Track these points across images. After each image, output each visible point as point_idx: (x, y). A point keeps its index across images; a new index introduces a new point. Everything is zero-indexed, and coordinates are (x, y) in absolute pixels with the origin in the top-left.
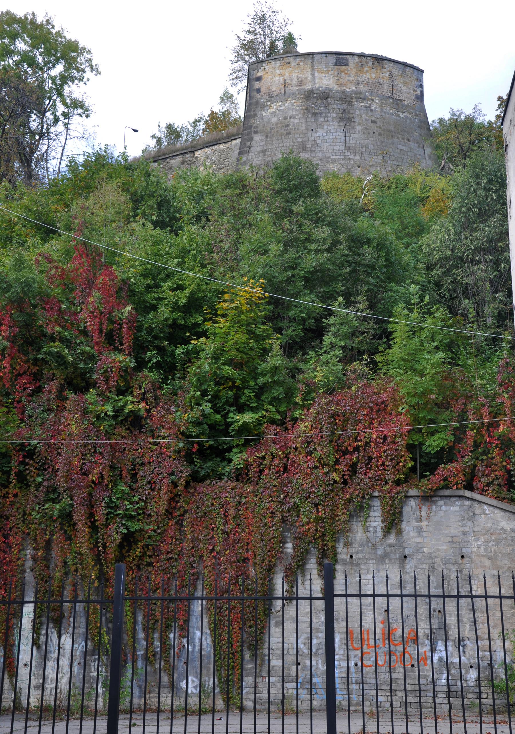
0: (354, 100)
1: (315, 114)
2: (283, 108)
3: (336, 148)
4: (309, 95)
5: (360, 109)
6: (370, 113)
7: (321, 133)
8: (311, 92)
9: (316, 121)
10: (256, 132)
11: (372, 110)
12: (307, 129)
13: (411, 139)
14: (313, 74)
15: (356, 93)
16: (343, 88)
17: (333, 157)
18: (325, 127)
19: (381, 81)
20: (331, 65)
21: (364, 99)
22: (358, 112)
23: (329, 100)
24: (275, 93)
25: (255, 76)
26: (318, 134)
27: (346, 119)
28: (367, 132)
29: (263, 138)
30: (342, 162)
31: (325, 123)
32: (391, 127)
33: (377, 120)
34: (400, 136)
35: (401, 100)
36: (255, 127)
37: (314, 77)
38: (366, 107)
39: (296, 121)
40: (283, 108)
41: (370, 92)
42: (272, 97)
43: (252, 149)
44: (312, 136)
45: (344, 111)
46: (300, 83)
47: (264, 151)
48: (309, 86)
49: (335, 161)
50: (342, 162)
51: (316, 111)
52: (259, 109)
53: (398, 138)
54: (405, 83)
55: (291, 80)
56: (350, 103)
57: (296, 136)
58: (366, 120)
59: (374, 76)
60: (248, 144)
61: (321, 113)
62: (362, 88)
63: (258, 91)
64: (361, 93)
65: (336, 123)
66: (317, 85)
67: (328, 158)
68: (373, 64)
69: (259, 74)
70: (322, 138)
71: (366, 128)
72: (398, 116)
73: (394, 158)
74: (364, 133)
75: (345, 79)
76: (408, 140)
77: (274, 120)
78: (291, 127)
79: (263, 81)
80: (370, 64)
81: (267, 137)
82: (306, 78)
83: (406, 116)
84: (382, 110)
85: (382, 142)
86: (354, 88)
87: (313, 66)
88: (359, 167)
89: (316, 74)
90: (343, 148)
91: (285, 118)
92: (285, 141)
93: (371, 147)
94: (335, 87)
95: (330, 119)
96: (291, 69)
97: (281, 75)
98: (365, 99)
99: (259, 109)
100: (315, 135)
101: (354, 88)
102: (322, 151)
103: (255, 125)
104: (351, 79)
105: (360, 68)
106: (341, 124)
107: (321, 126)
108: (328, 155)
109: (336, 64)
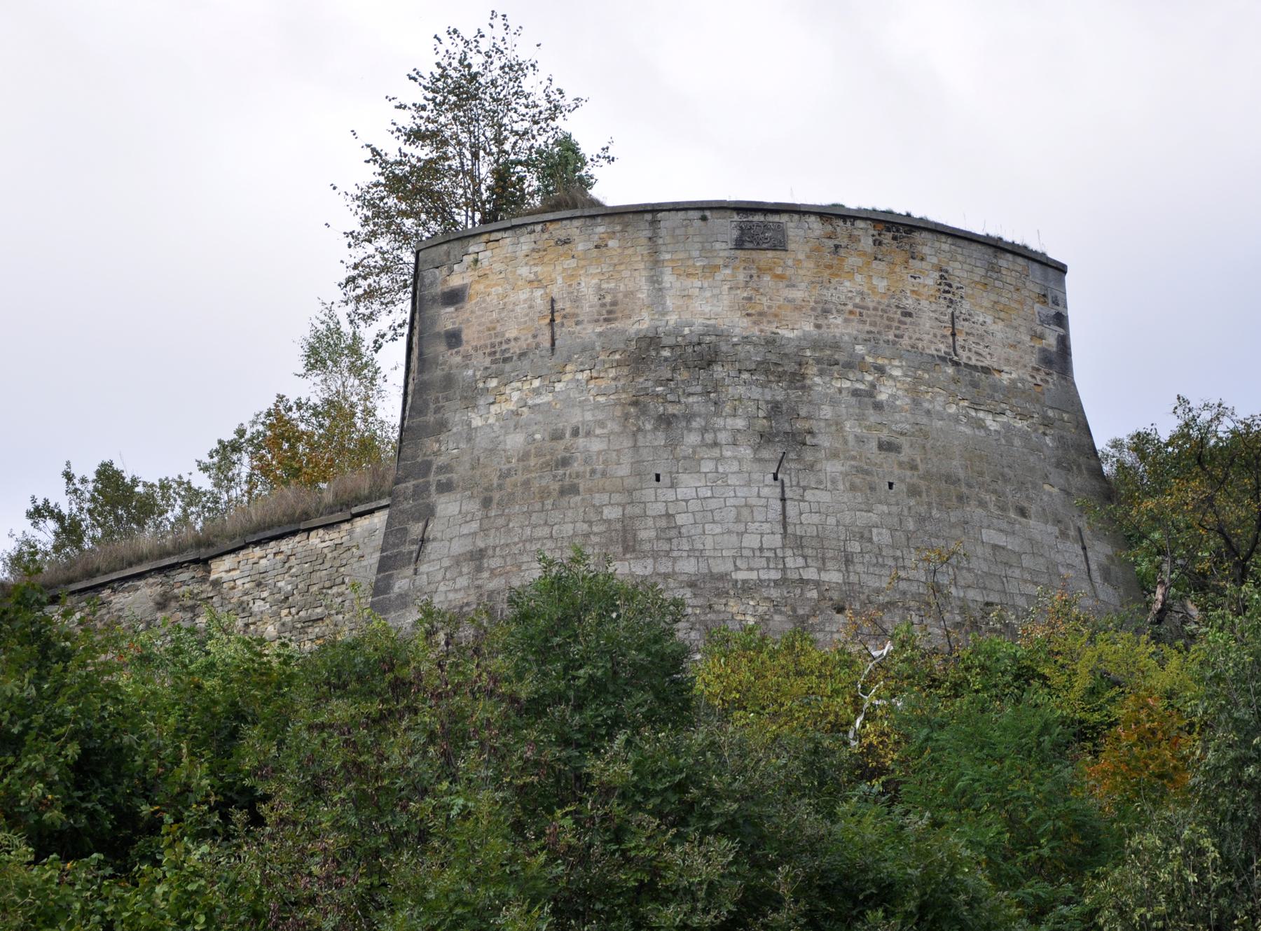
0: (812, 370)
1: (666, 421)
2: (546, 398)
3: (751, 541)
4: (643, 352)
5: (834, 402)
6: (873, 417)
7: (689, 486)
8: (651, 341)
9: (672, 444)
10: (446, 487)
11: (878, 406)
12: (638, 474)
13: (1033, 509)
14: (655, 280)
15: (816, 345)
16: (769, 328)
17: (740, 576)
18: (707, 466)
19: (909, 303)
20: (722, 249)
21: (849, 366)
22: (827, 411)
23: (719, 371)
24: (515, 348)
25: (439, 289)
26: (681, 492)
27: (784, 437)
28: (863, 482)
29: (473, 506)
30: (775, 593)
31: (704, 453)
32: (956, 466)
33: (902, 440)
34: (990, 498)
35: (986, 370)
36: (444, 469)
37: (658, 290)
38: (855, 393)
39: (596, 446)
40: (546, 398)
41: (871, 340)
42: (503, 360)
43: (430, 547)
44: (656, 500)
45: (775, 409)
46: (609, 312)
47: (477, 557)
48: (642, 323)
49: (746, 589)
50: (775, 593)
51: (672, 409)
52: (457, 404)
53: (982, 504)
54: (998, 310)
55: (576, 300)
56: (797, 379)
57: (599, 499)
58: (860, 440)
59: (881, 285)
60: (416, 529)
61: (689, 418)
62: (838, 327)
63: (454, 338)
64: (836, 346)
65: (746, 452)
66: (673, 319)
67: (722, 577)
68: (878, 243)
69: (455, 281)
70: (693, 505)
71: (860, 470)
72: (980, 425)
73: (970, 578)
74: (853, 488)
75: (773, 294)
76: (1023, 512)
77: (515, 441)
78: (576, 467)
79: (469, 305)
80: (867, 243)
81: (487, 503)
82: (629, 294)
83: (1008, 428)
84: (916, 403)
85: (921, 520)
86: (809, 327)
87: (655, 252)
88: (840, 610)
89: (668, 278)
90: (777, 540)
91: (557, 436)
92: (556, 516)
93: (881, 536)
94: (739, 325)
95: (723, 437)
96: (572, 263)
97: (536, 282)
98: (855, 364)
99: (457, 404)
100: (670, 495)
101: (809, 327)
102: (698, 554)
103: (441, 460)
104: (798, 294)
105: (828, 259)
106: (765, 454)
107: (692, 463)
108: (719, 567)
109: (739, 245)
